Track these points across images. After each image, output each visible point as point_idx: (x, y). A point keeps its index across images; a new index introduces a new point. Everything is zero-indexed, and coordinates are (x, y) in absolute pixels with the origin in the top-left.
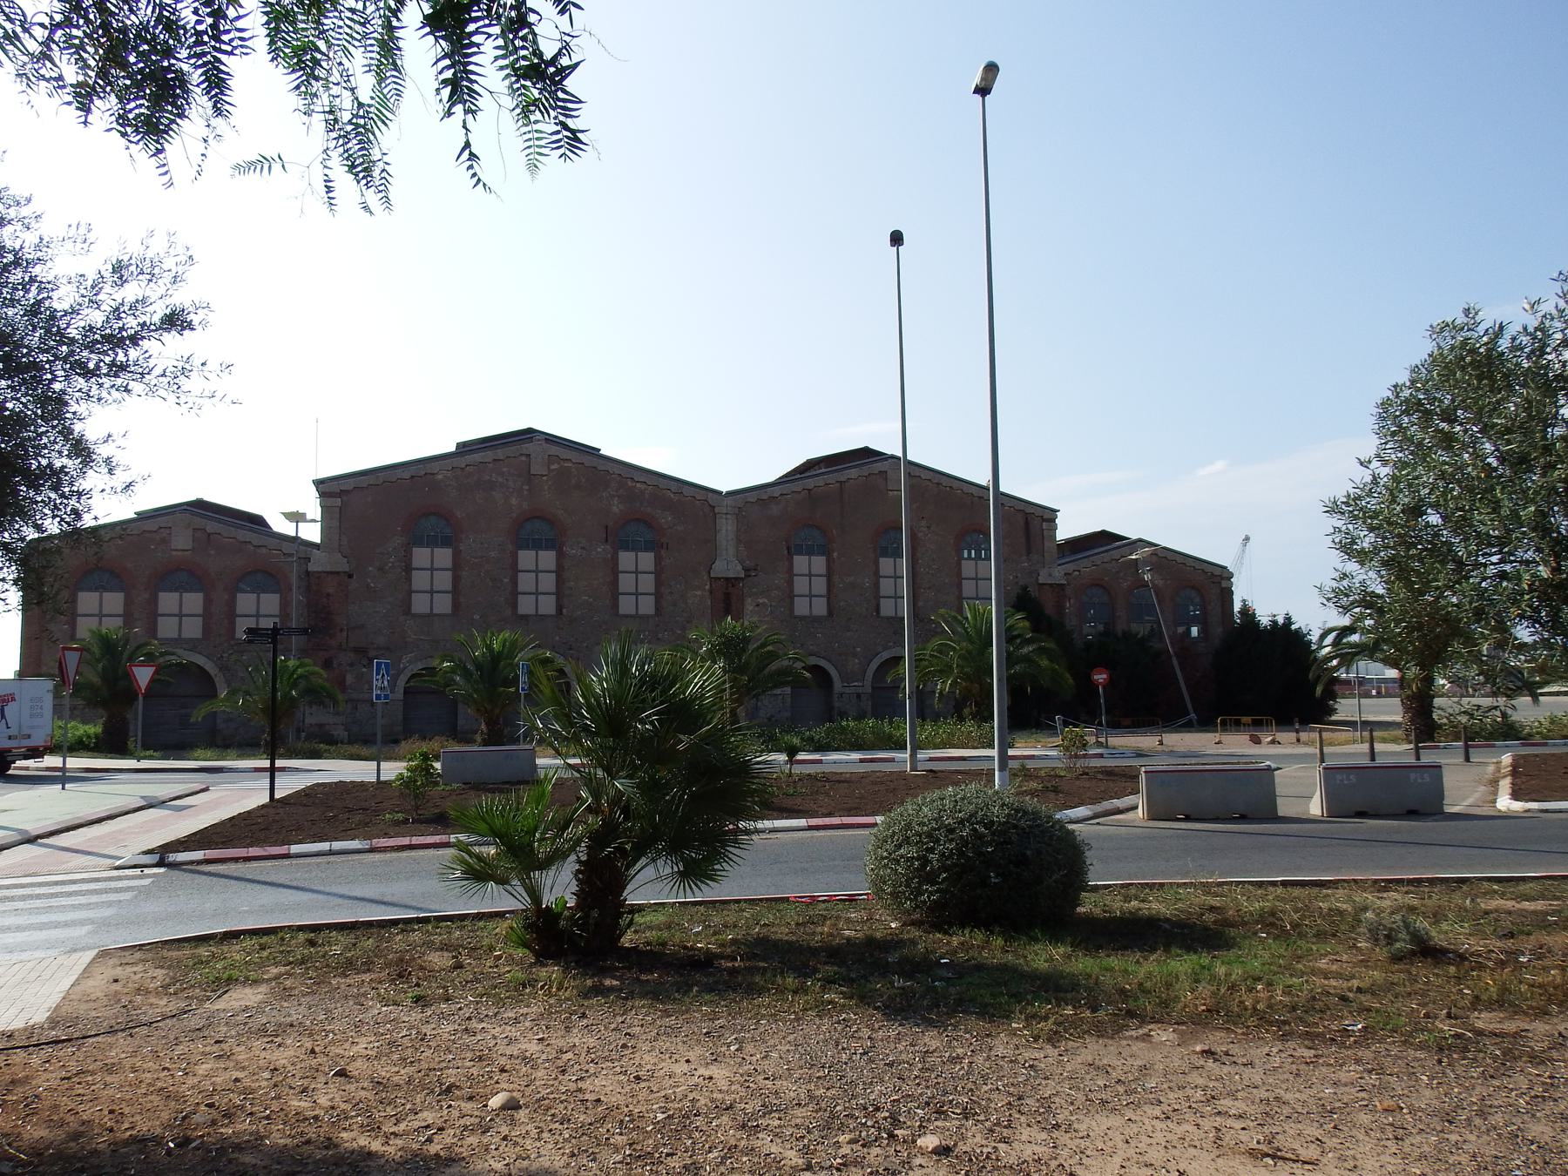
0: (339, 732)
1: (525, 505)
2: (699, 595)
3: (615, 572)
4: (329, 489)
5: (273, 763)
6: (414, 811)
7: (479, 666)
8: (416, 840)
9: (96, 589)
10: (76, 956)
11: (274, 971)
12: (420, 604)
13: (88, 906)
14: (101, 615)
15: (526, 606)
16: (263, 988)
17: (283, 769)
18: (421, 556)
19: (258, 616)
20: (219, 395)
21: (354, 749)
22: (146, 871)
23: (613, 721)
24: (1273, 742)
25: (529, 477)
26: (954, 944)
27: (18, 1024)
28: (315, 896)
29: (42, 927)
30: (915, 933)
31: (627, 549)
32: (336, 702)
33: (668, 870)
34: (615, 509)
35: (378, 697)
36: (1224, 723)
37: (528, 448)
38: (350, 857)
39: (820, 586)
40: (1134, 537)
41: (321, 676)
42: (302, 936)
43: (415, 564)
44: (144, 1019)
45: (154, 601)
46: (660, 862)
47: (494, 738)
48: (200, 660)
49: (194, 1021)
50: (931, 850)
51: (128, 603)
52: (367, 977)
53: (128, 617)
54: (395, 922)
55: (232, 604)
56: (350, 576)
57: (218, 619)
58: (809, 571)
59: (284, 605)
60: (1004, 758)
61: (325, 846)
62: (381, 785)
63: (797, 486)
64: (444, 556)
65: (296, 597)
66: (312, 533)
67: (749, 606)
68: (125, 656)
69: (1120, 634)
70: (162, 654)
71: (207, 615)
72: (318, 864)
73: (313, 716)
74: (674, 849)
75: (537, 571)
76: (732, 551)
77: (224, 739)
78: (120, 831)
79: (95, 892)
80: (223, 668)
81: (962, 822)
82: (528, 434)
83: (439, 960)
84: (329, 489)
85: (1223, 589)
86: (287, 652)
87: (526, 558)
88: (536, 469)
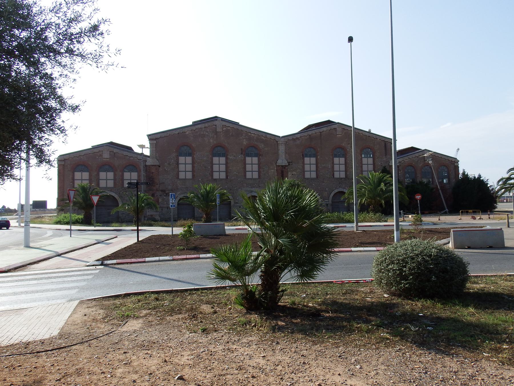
0: (158, 218)
1: (215, 142)
2: (273, 172)
3: (245, 164)
4: (152, 138)
5: (138, 228)
6: (189, 246)
7: (202, 196)
8: (188, 256)
9: (80, 171)
10: (71, 303)
11: (144, 312)
12: (182, 176)
13: (77, 281)
14: (82, 180)
15: (216, 176)
16: (141, 321)
17: (141, 230)
18: (182, 159)
19: (131, 180)
20: (115, 64)
21: (163, 223)
22: (97, 267)
23: (275, 215)
24: (480, 219)
25: (216, 133)
26: (418, 306)
27: (47, 336)
28: (156, 278)
29: (61, 289)
30: (396, 300)
31: (249, 156)
32: (156, 208)
33: (296, 274)
34: (245, 143)
35: (171, 206)
36: (462, 212)
37: (216, 123)
38: (166, 262)
39: (314, 167)
40: (423, 149)
41: (152, 199)
42: (153, 296)
43: (180, 162)
44: (96, 335)
45: (98, 175)
46: (292, 272)
47: (208, 220)
48: (113, 194)
49: (115, 338)
50: (405, 267)
51: (90, 175)
52: (180, 316)
53: (90, 180)
54: (186, 290)
55: (123, 176)
56: (159, 167)
57: (118, 180)
58: (310, 162)
59: (139, 176)
60: (398, 225)
61: (157, 258)
62: (173, 236)
63: (305, 134)
64: (189, 159)
65: (143, 173)
66: (147, 152)
67: (290, 175)
68: (90, 192)
69: (418, 182)
70: (101, 192)
71: (115, 179)
72: (155, 265)
73: (149, 212)
74: (299, 265)
75: (219, 164)
76: (284, 156)
77: (122, 220)
78: (89, 252)
79: (80, 275)
80: (121, 197)
81: (417, 255)
82: (216, 118)
83: (206, 308)
84: (152, 138)
85: (455, 166)
86: (141, 191)
87: (216, 160)
88: (219, 130)
